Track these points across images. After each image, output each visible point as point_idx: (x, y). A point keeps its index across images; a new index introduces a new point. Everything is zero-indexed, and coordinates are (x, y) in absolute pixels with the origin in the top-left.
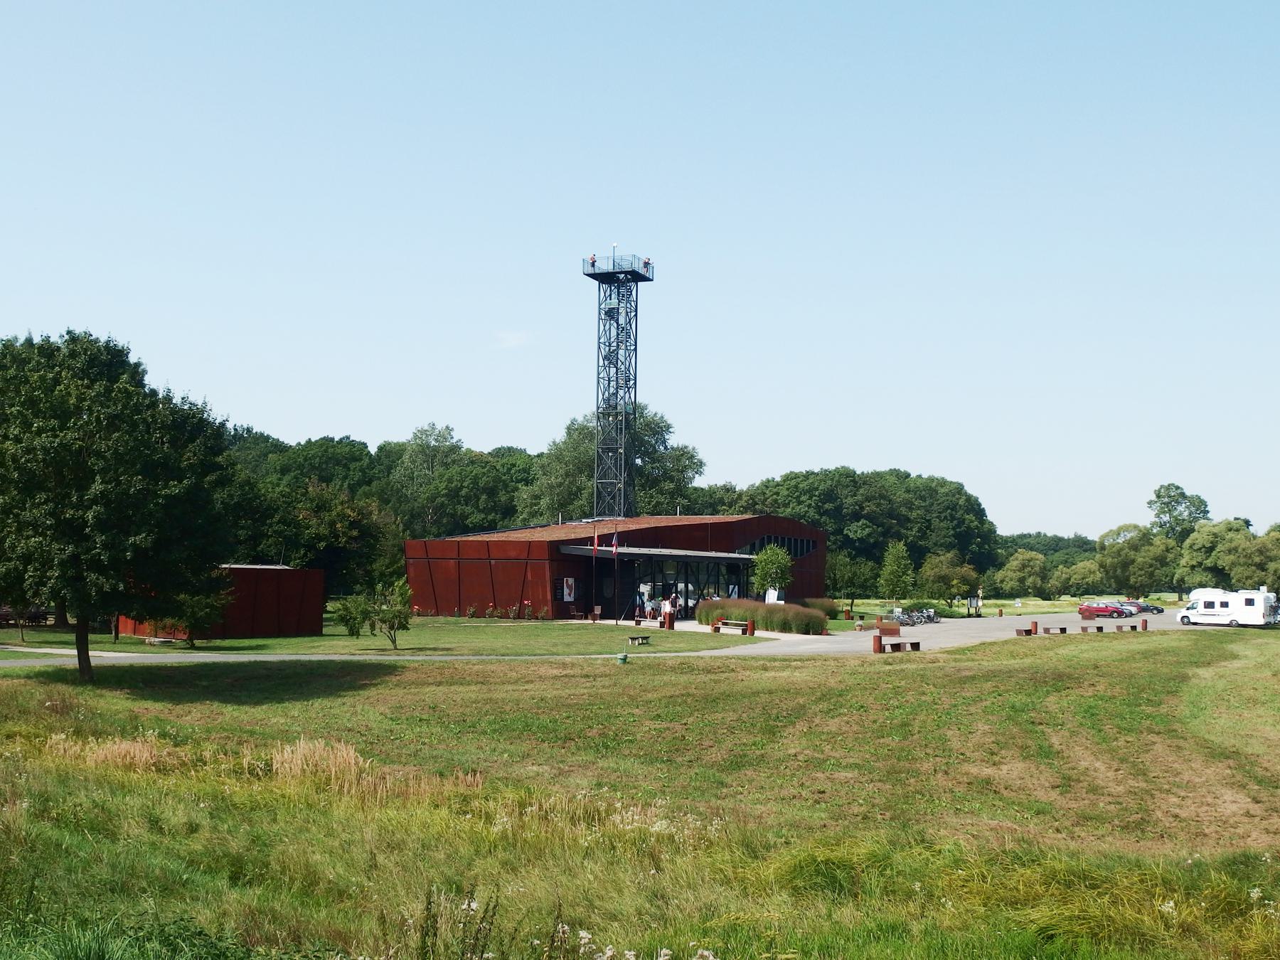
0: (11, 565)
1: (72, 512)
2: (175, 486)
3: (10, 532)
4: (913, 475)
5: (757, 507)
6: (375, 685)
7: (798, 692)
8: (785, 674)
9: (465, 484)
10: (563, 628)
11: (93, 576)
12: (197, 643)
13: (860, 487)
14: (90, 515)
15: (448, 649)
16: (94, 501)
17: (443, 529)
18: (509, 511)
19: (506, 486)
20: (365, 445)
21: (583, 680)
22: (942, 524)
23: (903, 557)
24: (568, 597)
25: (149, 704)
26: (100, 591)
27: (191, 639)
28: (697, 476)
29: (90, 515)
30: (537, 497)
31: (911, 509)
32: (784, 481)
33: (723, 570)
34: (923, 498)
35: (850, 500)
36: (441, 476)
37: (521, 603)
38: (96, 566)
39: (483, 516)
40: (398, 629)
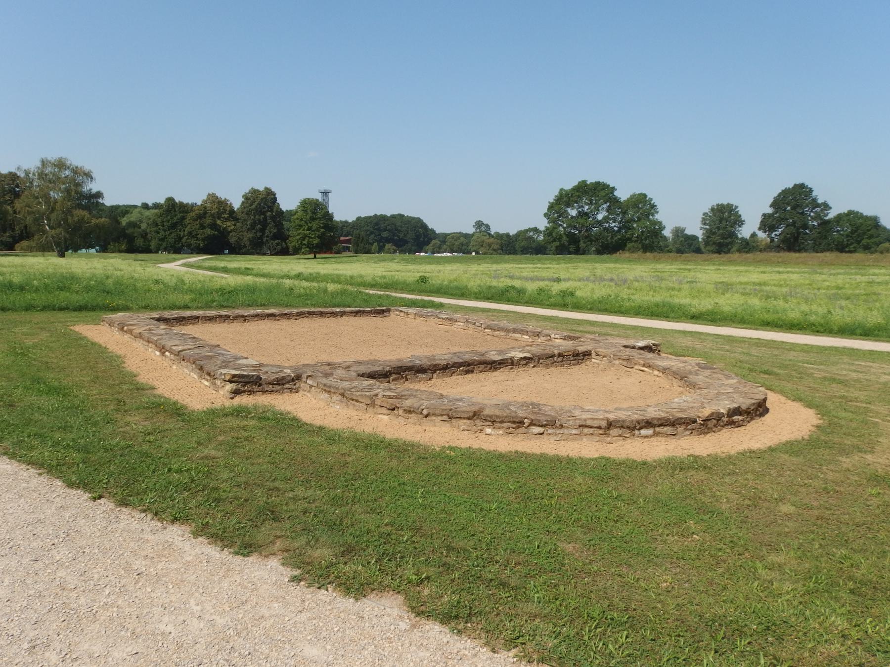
20: (317, 200)
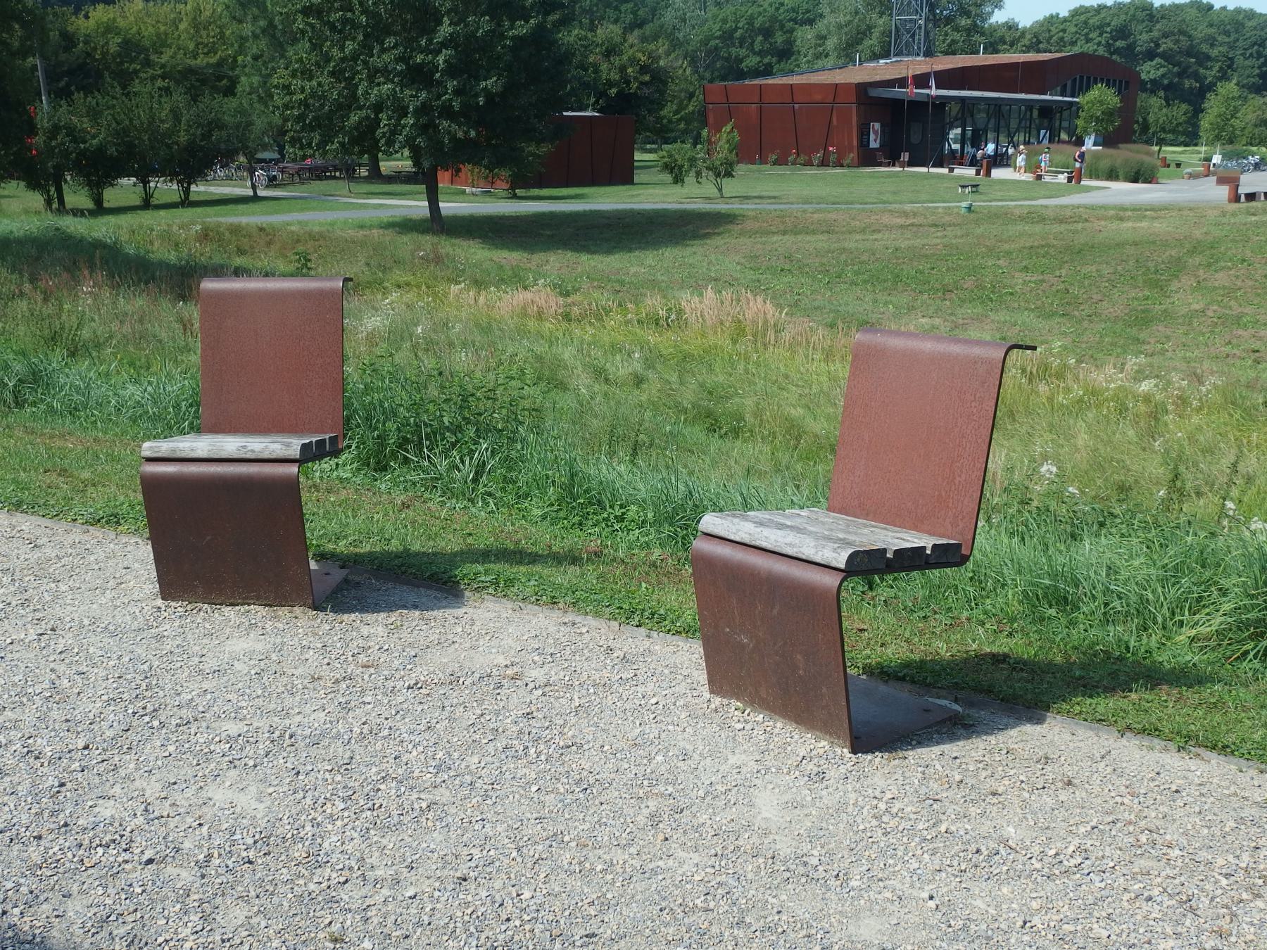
0: (364, 113)
1: (422, 57)
2: (522, 26)
3: (361, 79)
4: (1217, 7)
5: (1041, 46)
6: (719, 234)
7: (1165, 245)
8: (1144, 224)
9: (740, 25)
10: (872, 176)
11: (445, 124)
12: (519, 192)
13: (1158, 22)
14: (441, 59)
15: (775, 198)
16: (444, 45)
17: (716, 74)
18: (786, 53)
19: (782, 27)
21: (933, 230)
22: (1246, 62)
23: (1233, 98)
24: (874, 144)
25: (505, 254)
26: (453, 138)
27: (513, 187)
28: (996, 10)
29: (441, 59)
30: (824, 38)
31: (1212, 45)
32: (1073, 16)
33: (1035, 113)
34: (1227, 33)
35: (1145, 37)
36: (715, 17)
37: (825, 149)
38: (447, 112)
39: (758, 59)
40: (724, 177)
